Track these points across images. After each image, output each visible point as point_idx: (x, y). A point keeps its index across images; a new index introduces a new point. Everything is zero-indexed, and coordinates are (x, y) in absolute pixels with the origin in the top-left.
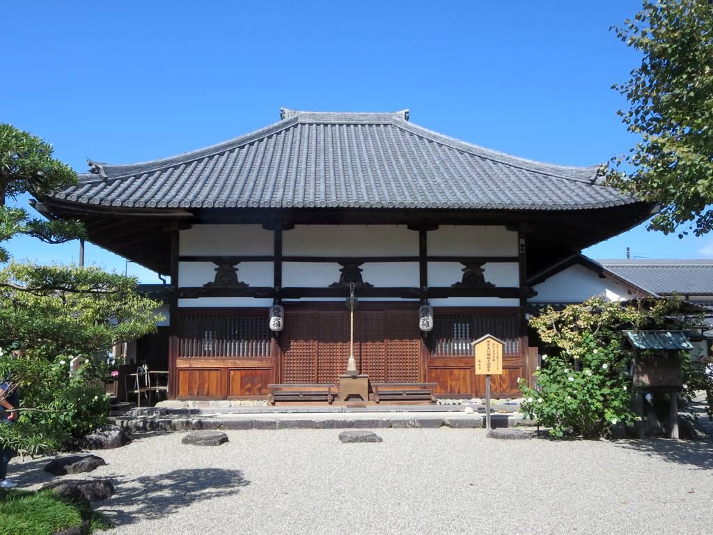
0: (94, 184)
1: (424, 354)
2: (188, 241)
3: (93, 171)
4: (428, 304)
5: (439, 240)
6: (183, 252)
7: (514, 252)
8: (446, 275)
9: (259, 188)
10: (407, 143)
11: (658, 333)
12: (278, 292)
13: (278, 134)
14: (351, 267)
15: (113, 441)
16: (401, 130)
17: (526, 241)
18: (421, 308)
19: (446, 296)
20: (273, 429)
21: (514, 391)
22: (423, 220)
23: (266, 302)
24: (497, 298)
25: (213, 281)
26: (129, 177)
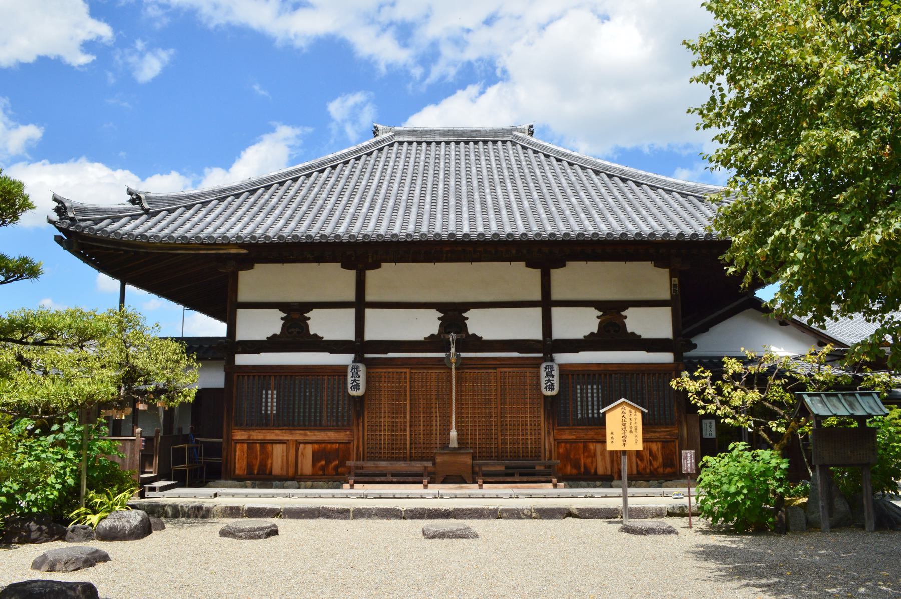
0: (134, 217)
1: (549, 424)
2: (253, 283)
3: (133, 201)
4: (552, 360)
5: (569, 279)
6: (243, 297)
7: (666, 295)
8: (576, 323)
9: (323, 217)
10: (529, 163)
11: (843, 395)
12: (359, 346)
13: (368, 154)
14: (453, 314)
15: (131, 530)
16: (523, 147)
17: (680, 281)
18: (543, 366)
19: (576, 351)
20: (344, 519)
21: (668, 470)
22: (546, 254)
23: (345, 359)
24: (645, 353)
25: (278, 332)
26: (177, 208)
